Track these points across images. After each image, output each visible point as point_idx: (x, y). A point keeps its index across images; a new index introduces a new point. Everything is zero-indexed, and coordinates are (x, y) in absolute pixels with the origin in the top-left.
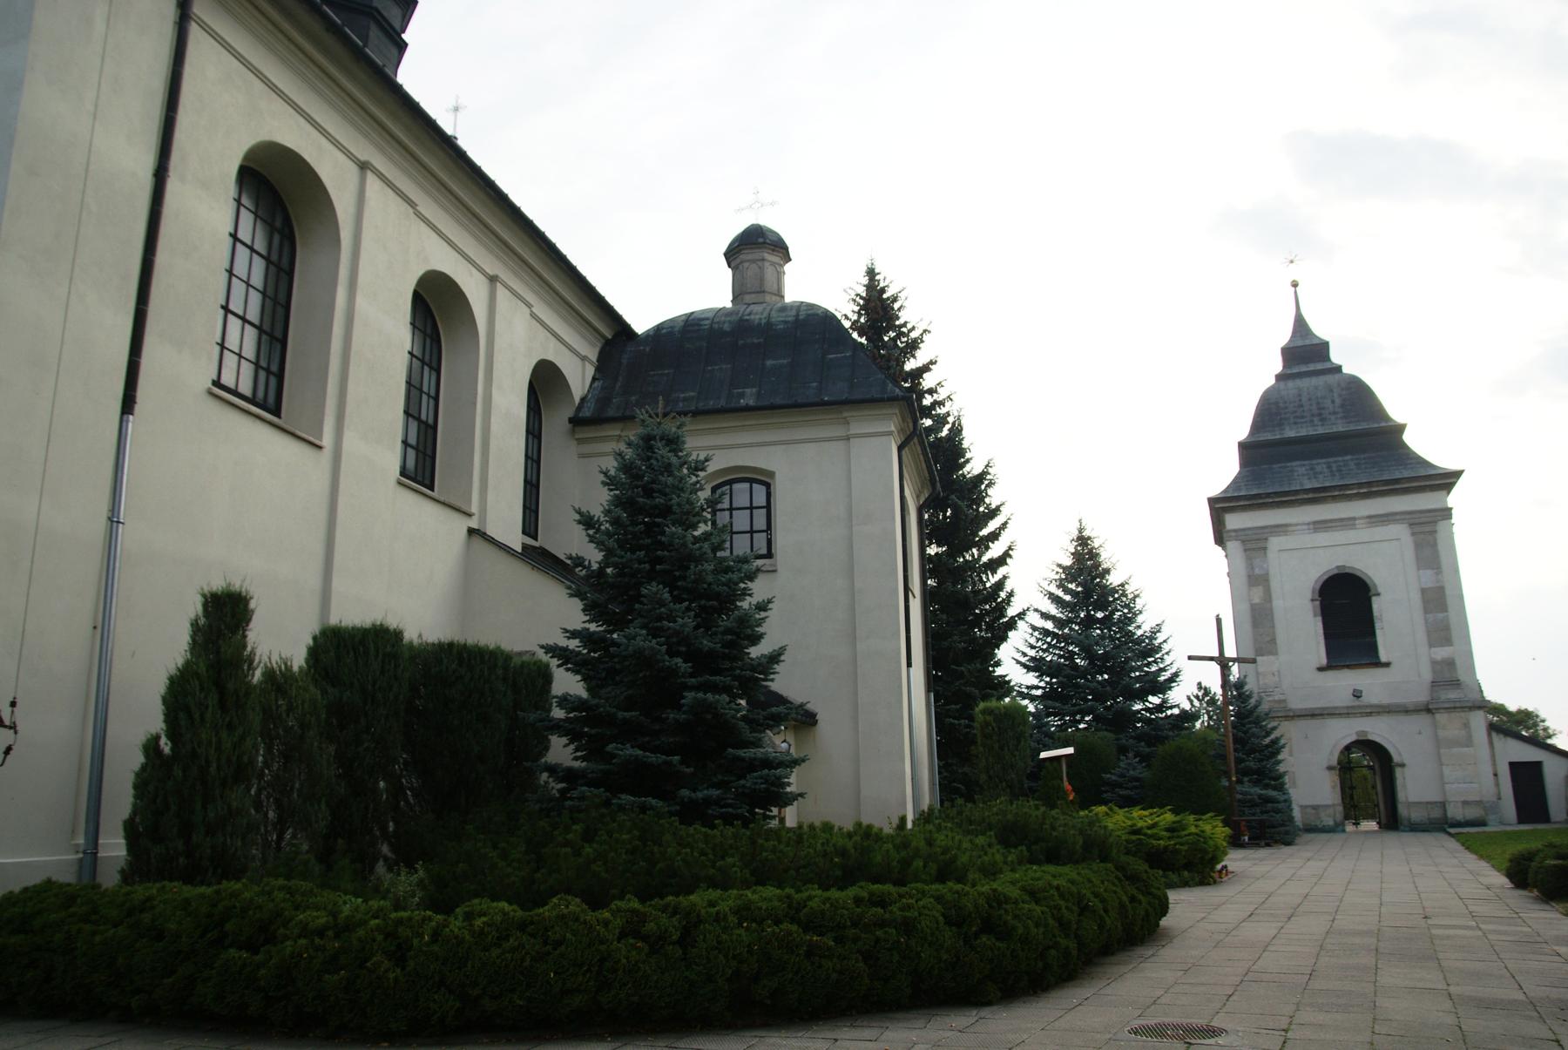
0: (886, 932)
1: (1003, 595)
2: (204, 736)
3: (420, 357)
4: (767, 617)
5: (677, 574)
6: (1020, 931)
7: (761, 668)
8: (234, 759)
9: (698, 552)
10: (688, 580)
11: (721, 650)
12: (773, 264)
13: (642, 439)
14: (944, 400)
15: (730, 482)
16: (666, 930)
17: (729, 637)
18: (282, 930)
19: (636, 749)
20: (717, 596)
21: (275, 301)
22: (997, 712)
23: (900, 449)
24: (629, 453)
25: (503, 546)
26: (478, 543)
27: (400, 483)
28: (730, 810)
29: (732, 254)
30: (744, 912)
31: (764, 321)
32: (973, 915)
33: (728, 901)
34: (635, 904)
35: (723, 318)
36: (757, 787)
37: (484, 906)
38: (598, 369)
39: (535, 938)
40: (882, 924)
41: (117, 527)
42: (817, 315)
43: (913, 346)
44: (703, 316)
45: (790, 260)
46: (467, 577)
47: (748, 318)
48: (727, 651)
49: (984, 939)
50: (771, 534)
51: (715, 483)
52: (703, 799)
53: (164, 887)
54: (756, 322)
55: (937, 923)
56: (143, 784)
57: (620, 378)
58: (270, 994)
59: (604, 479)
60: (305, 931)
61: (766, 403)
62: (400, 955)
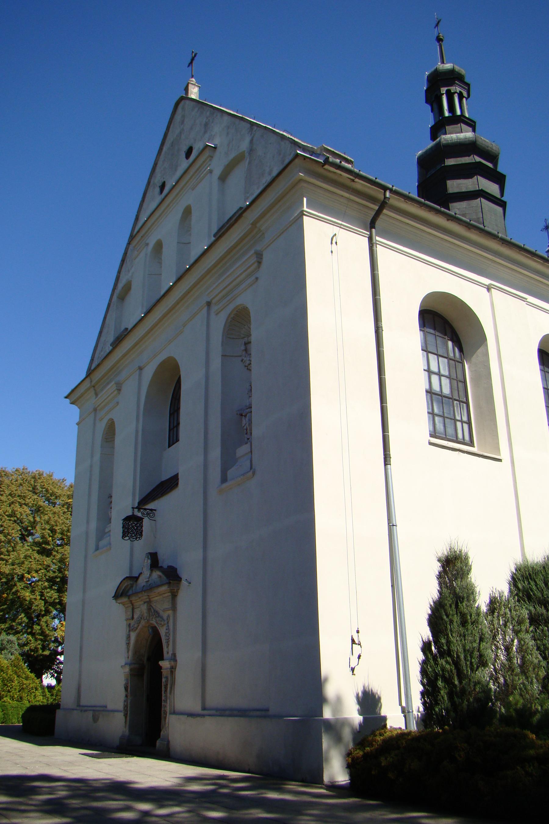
41: (393, 528)
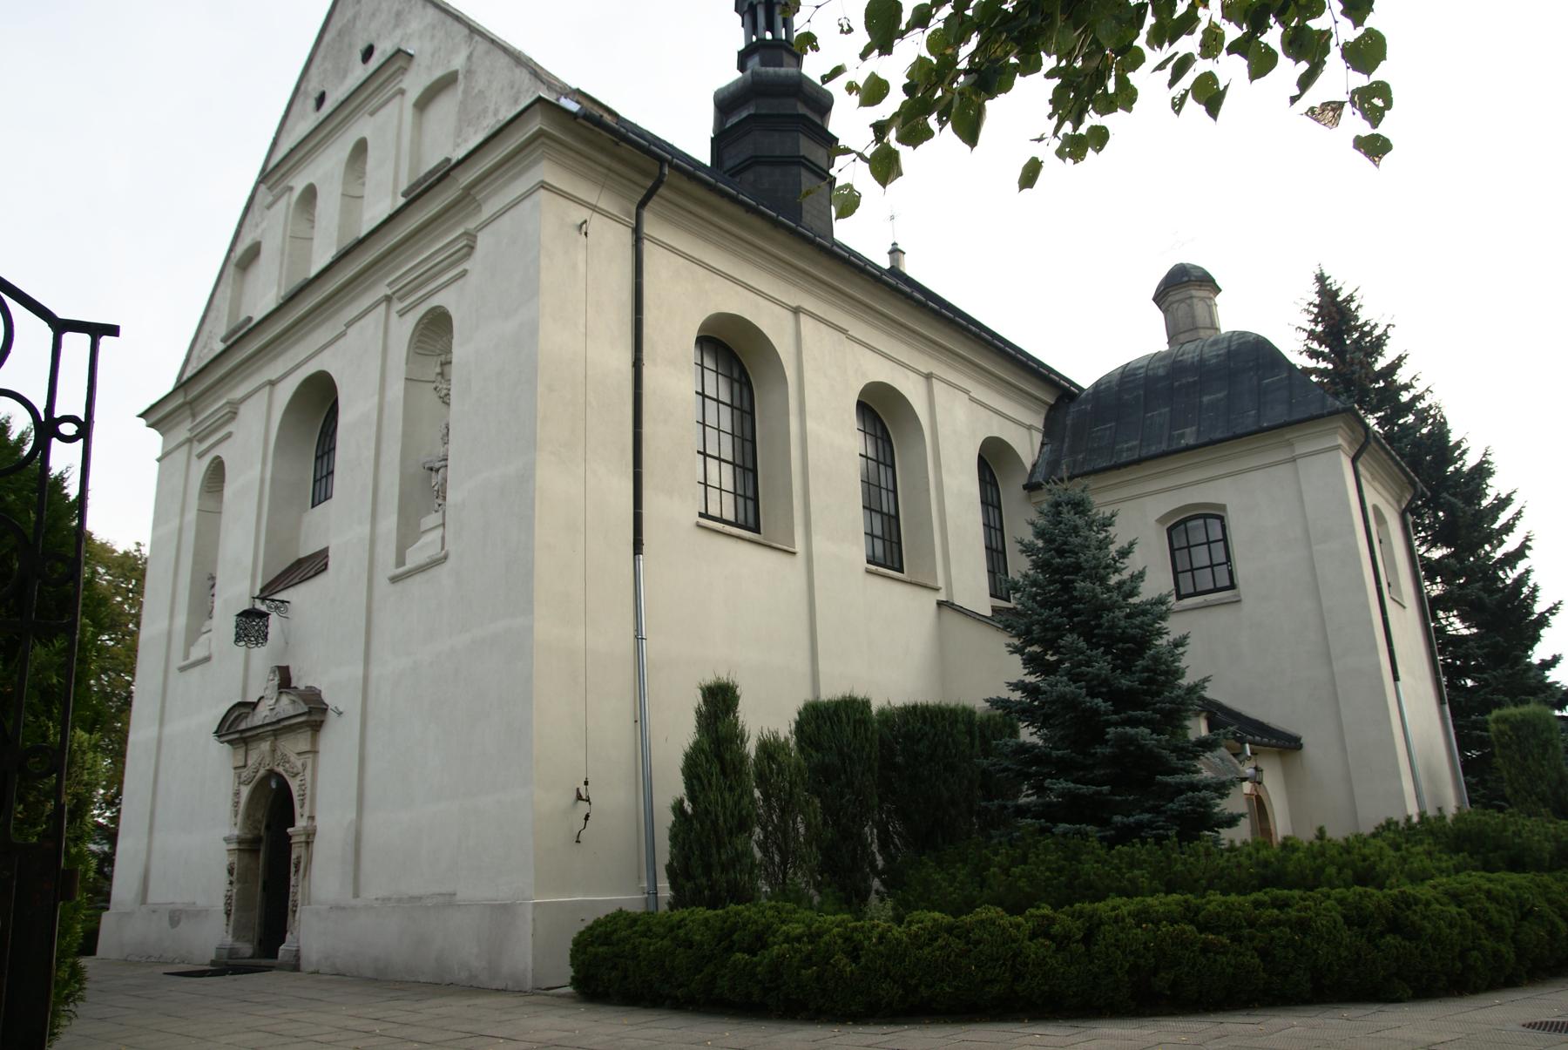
0: (1281, 931)
1: (1525, 590)
2: (712, 797)
3: (875, 458)
4: (1185, 652)
5: (1093, 623)
6: (1430, 931)
7: (1180, 700)
8: (736, 813)
9: (1108, 602)
10: (1104, 627)
11: (1140, 687)
12: (1202, 299)
13: (1052, 506)
14: (1423, 393)
16: (1070, 931)
17: (1146, 675)
18: (771, 938)
19: (1070, 783)
20: (1133, 639)
21: (743, 439)
22: (1512, 719)
23: (1354, 461)
24: (1042, 522)
25: (969, 613)
26: (947, 612)
27: (868, 572)
28: (1161, 831)
29: (1161, 298)
30: (1142, 916)
31: (1196, 359)
32: (1376, 916)
33: (1126, 906)
34: (1046, 910)
35: (1157, 364)
36: (1183, 809)
37: (922, 917)
39: (959, 939)
40: (1277, 923)
42: (1249, 342)
43: (1378, 345)
44: (1138, 365)
45: (1220, 290)
46: (941, 640)
47: (1180, 358)
48: (1145, 687)
49: (1388, 938)
50: (1231, 565)
51: (1169, 525)
52: (1134, 823)
53: (693, 911)
54: (1190, 361)
55: (1335, 922)
56: (674, 838)
57: (1067, 440)
58: (767, 985)
59: (1021, 547)
60: (788, 939)
61: (1207, 440)
62: (854, 953)
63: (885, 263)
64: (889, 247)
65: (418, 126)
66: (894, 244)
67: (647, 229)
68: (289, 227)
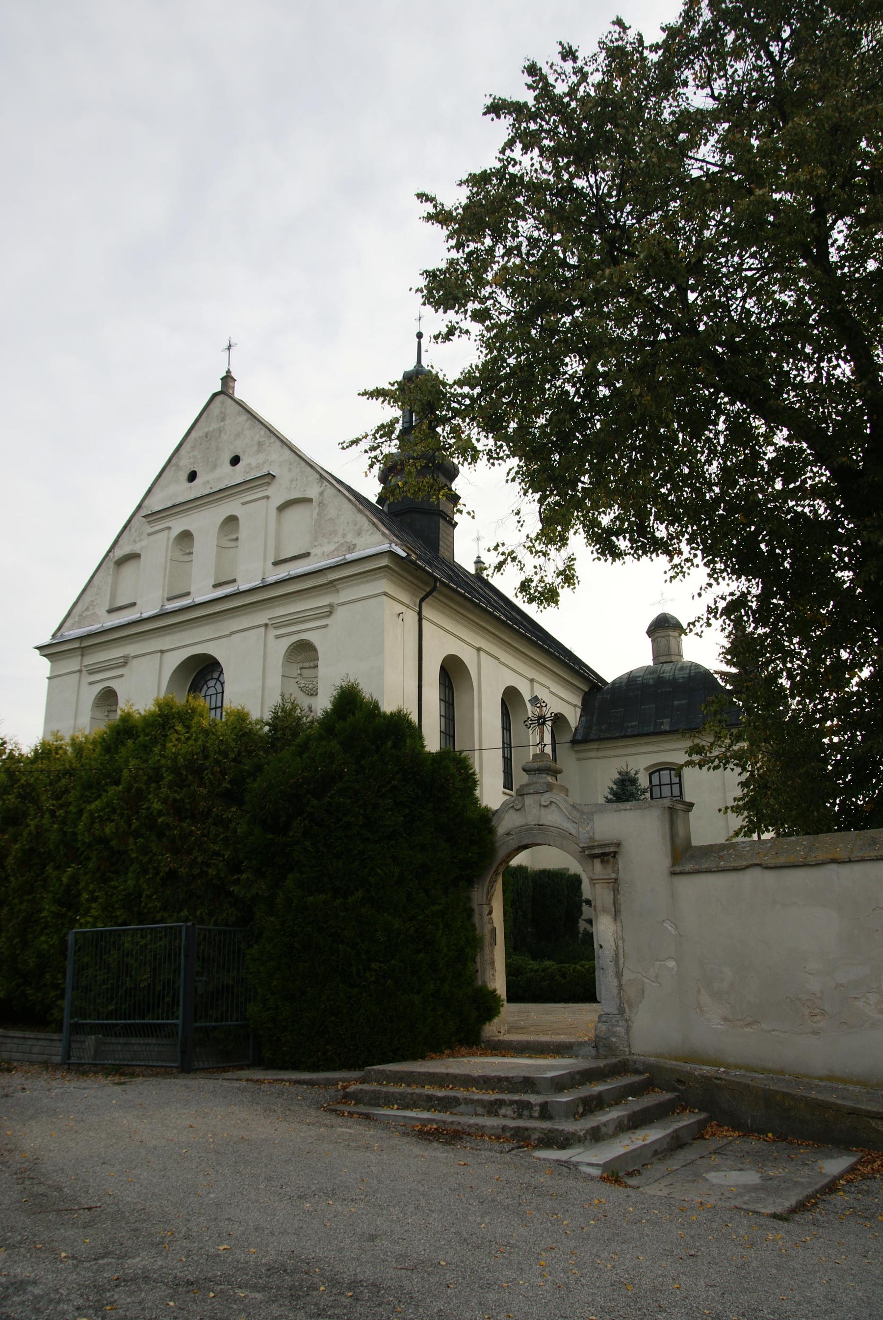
12: (675, 637)
15: (659, 771)
38: (582, 710)
63: (472, 570)
64: (475, 559)
65: (279, 520)
66: (479, 557)
67: (424, 613)
68: (169, 554)
